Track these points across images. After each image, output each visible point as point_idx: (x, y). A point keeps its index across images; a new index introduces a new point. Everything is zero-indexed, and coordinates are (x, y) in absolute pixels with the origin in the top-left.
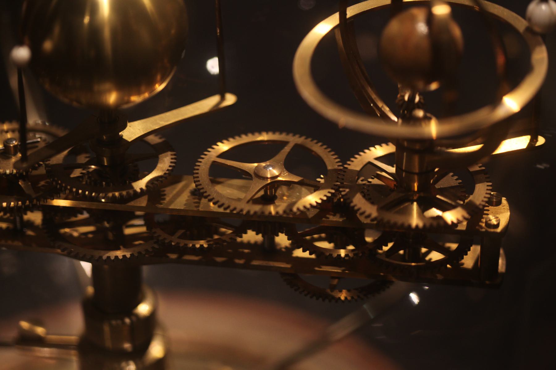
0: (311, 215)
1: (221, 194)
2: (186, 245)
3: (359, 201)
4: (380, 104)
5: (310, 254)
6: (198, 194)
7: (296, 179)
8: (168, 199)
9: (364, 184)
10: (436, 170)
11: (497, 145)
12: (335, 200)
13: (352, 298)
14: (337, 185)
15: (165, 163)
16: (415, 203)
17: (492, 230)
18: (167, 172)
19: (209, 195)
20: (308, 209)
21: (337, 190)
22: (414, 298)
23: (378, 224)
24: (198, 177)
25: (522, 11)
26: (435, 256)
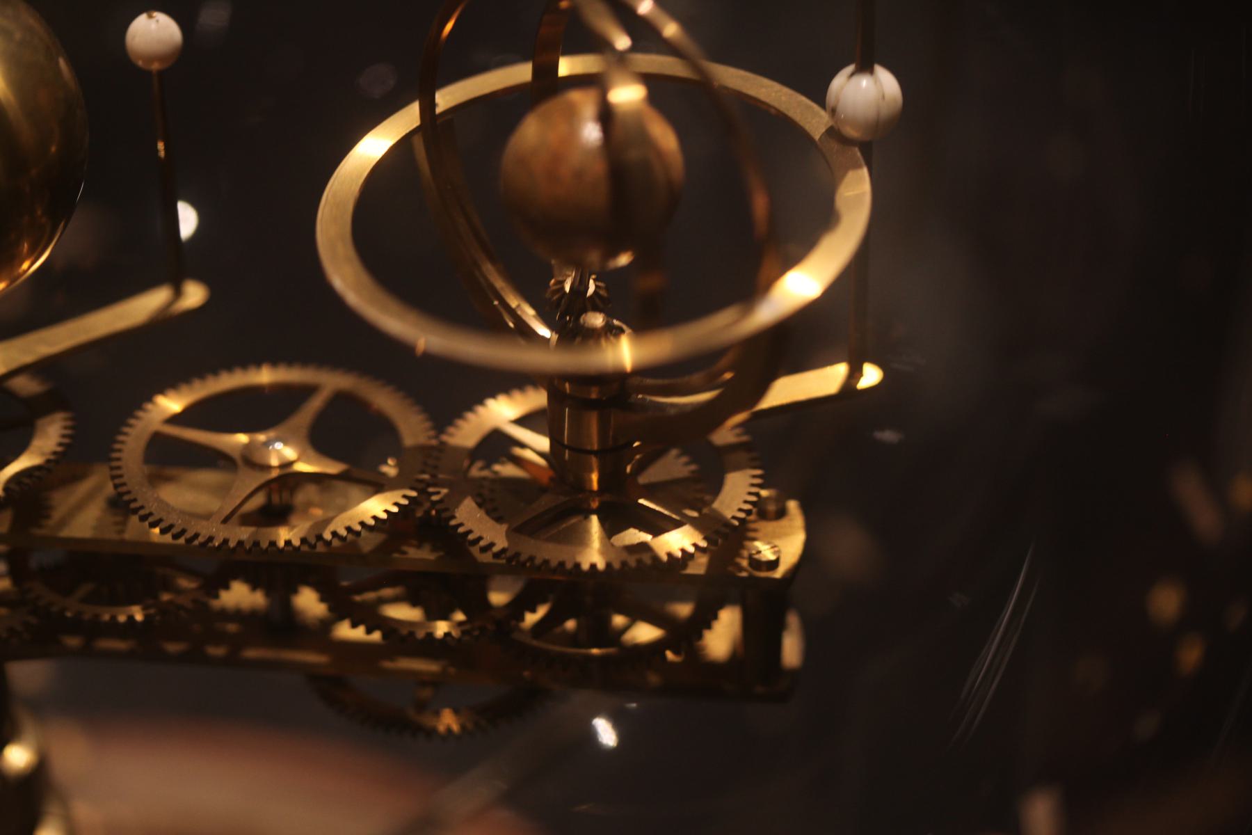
0: (369, 543)
1: (167, 505)
2: (97, 616)
3: (469, 516)
4: (514, 302)
5: (369, 631)
6: (121, 505)
7: (333, 468)
8: (57, 515)
9: (484, 479)
10: (636, 444)
11: (762, 389)
12: (419, 514)
13: (463, 727)
14: (422, 481)
15: (49, 438)
16: (594, 520)
17: (763, 574)
18: (52, 457)
19: (142, 507)
20: (358, 534)
21: (422, 492)
22: (606, 733)
23: (511, 564)
24: (119, 468)
25: (818, 93)
26: (645, 633)
